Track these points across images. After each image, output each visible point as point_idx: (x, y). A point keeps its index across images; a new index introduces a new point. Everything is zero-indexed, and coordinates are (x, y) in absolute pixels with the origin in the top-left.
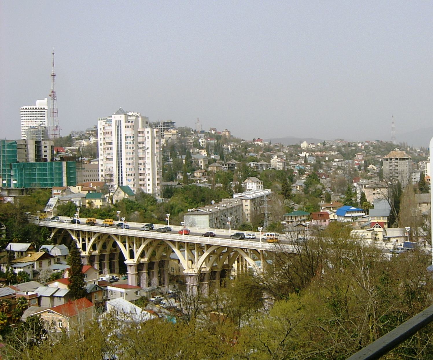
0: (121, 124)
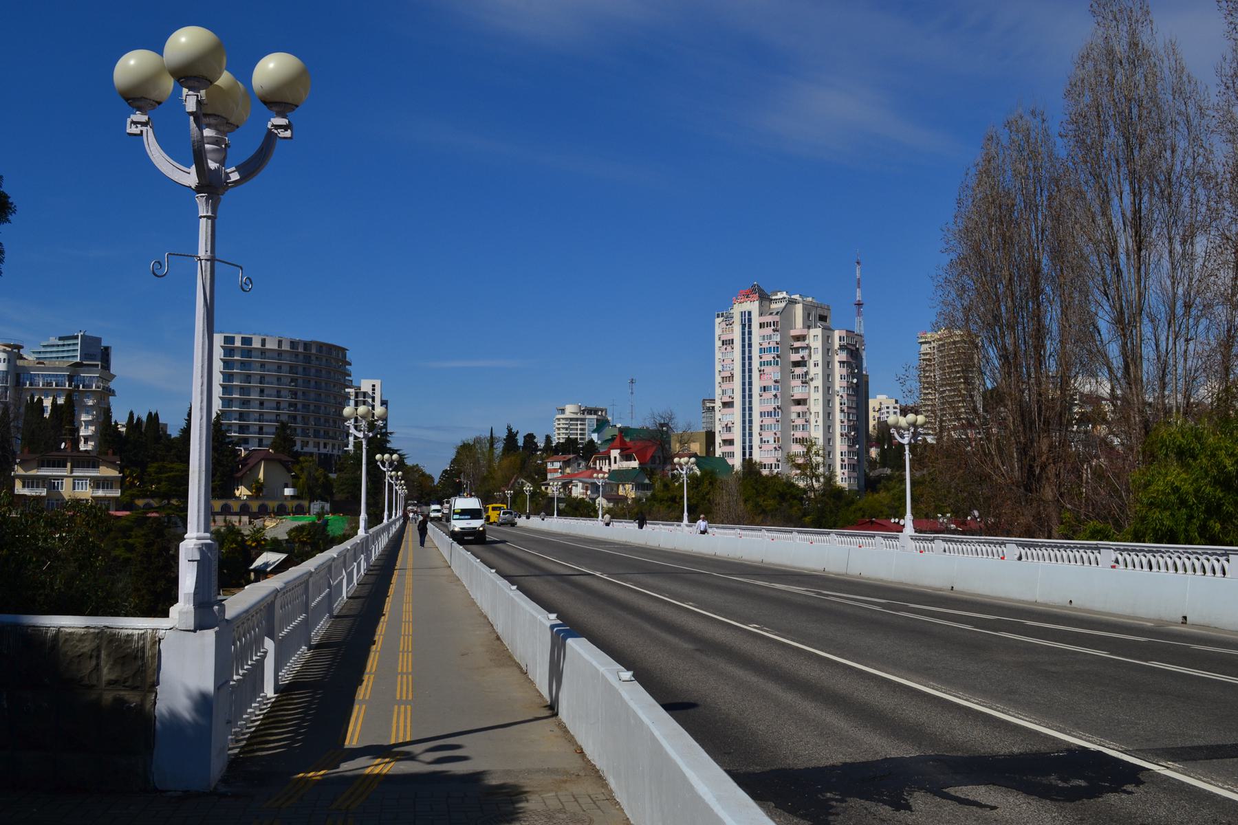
0: (750, 320)
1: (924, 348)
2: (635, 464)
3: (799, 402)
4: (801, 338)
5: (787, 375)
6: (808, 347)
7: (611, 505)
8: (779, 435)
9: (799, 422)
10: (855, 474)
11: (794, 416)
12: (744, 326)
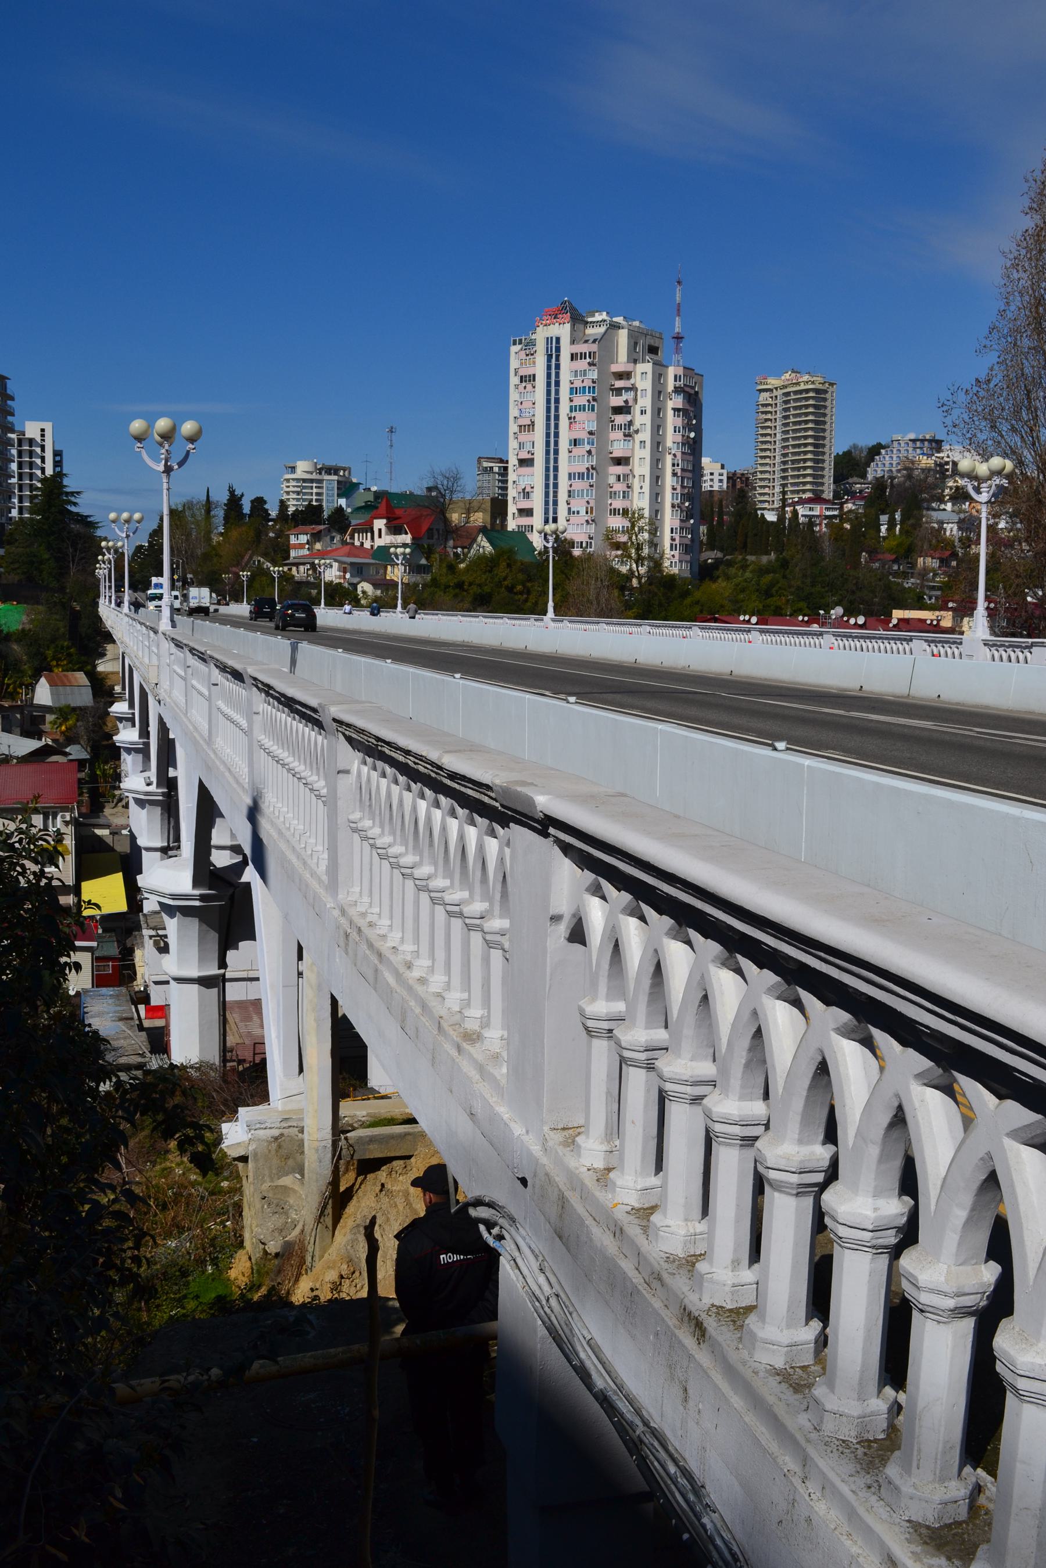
0: (558, 349)
1: (764, 397)
2: (407, 538)
3: (619, 461)
4: (625, 375)
5: (605, 425)
6: (633, 388)
7: (378, 592)
8: (592, 504)
9: (619, 487)
10: (688, 557)
11: (612, 480)
12: (549, 357)
